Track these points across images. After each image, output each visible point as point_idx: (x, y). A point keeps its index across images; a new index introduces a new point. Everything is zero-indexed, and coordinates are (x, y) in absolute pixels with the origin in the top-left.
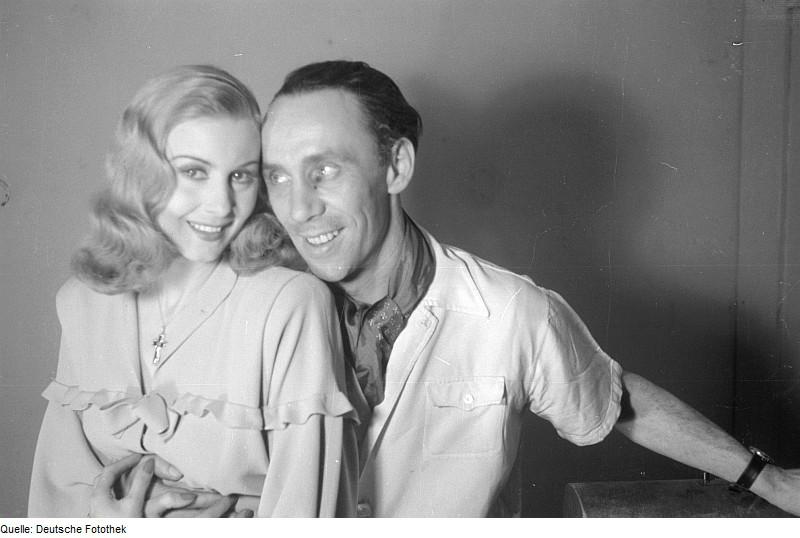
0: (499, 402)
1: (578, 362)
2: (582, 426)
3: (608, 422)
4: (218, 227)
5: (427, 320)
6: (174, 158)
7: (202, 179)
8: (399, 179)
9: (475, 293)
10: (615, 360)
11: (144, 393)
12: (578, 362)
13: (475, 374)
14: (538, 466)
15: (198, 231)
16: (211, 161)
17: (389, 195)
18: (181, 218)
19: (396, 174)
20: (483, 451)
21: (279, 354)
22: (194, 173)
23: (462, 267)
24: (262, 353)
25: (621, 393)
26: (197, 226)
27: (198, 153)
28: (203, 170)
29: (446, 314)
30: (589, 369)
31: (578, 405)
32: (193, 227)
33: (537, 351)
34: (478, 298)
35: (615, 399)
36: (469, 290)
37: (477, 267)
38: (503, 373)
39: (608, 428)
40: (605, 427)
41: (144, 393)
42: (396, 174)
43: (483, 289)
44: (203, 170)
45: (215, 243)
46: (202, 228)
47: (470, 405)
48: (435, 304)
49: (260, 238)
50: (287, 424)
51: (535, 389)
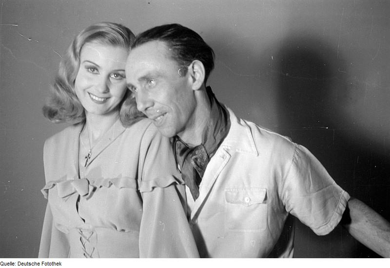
0: (261, 202)
1: (312, 186)
2: (322, 225)
3: (331, 224)
4: (102, 98)
5: (224, 155)
6: (151, 123)
7: (96, 74)
8: (196, 82)
9: (252, 143)
10: (345, 191)
11: (79, 178)
12: (312, 186)
13: (252, 186)
14: (287, 234)
15: (92, 99)
16: (100, 66)
17: (194, 91)
18: (84, 90)
19: (194, 80)
20: (256, 224)
21: (146, 162)
22: (94, 71)
23: (248, 130)
24: (140, 144)
25: (344, 209)
26: (92, 96)
27: (97, 63)
28: (97, 70)
29: (236, 154)
30: (321, 191)
31: (311, 210)
32: (90, 96)
33: (284, 177)
34: (253, 145)
35: (339, 211)
36: (249, 141)
37: (256, 129)
38: (266, 186)
39: (331, 227)
40: (329, 226)
41: (79, 178)
42: (194, 80)
43: (256, 141)
44: (97, 70)
45: (101, 106)
46: (94, 98)
47: (248, 204)
48: (229, 148)
49: (126, 106)
50: (153, 188)
51: (285, 196)
